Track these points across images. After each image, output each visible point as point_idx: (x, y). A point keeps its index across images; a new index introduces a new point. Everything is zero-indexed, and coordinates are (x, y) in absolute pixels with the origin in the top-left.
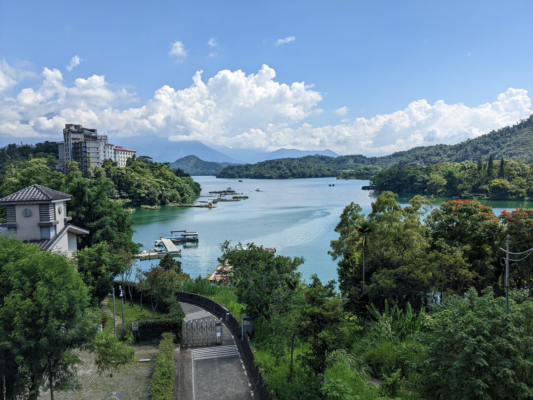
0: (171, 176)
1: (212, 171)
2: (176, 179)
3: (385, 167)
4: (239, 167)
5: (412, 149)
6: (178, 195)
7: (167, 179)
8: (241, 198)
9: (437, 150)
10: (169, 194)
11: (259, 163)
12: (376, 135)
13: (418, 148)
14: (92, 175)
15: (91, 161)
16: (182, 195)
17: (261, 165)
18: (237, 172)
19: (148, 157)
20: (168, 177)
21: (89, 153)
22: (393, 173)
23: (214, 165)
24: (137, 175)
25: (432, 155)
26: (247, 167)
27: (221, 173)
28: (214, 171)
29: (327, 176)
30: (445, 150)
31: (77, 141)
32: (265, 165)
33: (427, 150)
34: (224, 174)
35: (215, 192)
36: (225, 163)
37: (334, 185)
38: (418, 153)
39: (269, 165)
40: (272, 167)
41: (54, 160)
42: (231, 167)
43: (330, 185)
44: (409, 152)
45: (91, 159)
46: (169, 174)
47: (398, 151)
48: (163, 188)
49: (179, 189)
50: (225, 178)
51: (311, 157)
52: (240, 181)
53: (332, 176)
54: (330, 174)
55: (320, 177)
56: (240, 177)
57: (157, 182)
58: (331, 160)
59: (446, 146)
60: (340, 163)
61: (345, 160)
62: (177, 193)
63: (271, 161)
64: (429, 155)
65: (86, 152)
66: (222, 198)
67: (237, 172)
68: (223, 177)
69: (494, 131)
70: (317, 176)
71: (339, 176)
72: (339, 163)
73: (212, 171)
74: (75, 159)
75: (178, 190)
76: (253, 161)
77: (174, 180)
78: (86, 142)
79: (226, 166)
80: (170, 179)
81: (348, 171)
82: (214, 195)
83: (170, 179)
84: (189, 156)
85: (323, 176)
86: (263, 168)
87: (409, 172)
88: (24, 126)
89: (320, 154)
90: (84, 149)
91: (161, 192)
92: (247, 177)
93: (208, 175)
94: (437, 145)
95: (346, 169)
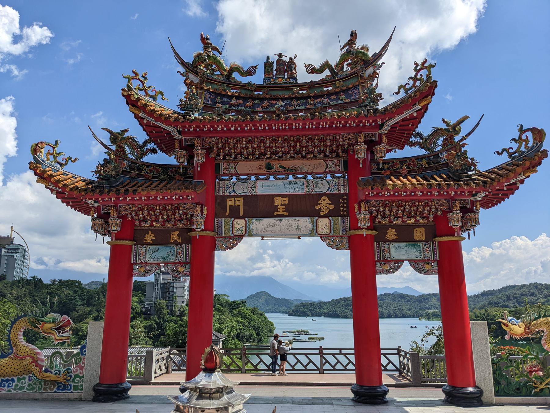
0: (249, 315)
1: (284, 308)
2: (253, 318)
3: (473, 307)
4: (311, 304)
5: (503, 288)
6: (255, 334)
7: (245, 318)
8: (316, 339)
9: (531, 289)
10: (247, 333)
11: (333, 300)
12: (37, 45)
13: (510, 286)
14: (178, 314)
15: (177, 300)
16: (258, 334)
17: (335, 302)
18: (310, 310)
19: (226, 295)
20: (246, 316)
21: (176, 292)
22: (479, 315)
23: (285, 302)
24: (218, 313)
25: (526, 295)
26: (321, 304)
27: (293, 311)
28: (285, 309)
29: (408, 317)
30: (540, 290)
31: (166, 281)
32: (339, 302)
33: (520, 288)
34: (297, 311)
35: (288, 332)
36: (296, 300)
37: (415, 327)
38: (509, 292)
39: (343, 302)
40: (346, 306)
41: (143, 298)
42: (304, 305)
43: (412, 327)
44: (500, 291)
45: (177, 298)
46: (247, 313)
47: (486, 290)
48: (241, 327)
49: (256, 328)
50: (297, 316)
51: (389, 294)
52: (313, 320)
53: (414, 317)
54: (412, 314)
55: (400, 317)
56: (313, 315)
57: (236, 321)
58: (411, 299)
59: (542, 285)
60: (422, 302)
61: (427, 299)
62: (254, 332)
63: (346, 298)
64: (522, 295)
65: (173, 291)
66: (296, 338)
67: (310, 310)
68: (295, 315)
69: (508, 198)
70: (396, 316)
71: (421, 316)
72: (421, 302)
73: (284, 308)
74: (163, 297)
75: (254, 329)
76: (326, 299)
77: (251, 319)
78: (174, 283)
79: (298, 303)
80: (248, 318)
81: (431, 311)
82: (288, 334)
83: (248, 318)
84: (260, 292)
85: (404, 316)
86: (338, 306)
87: (497, 315)
88: (99, 264)
89: (400, 292)
90: (171, 288)
91: (239, 331)
92: (320, 315)
93: (279, 312)
94: (531, 284)
95: (429, 309)
